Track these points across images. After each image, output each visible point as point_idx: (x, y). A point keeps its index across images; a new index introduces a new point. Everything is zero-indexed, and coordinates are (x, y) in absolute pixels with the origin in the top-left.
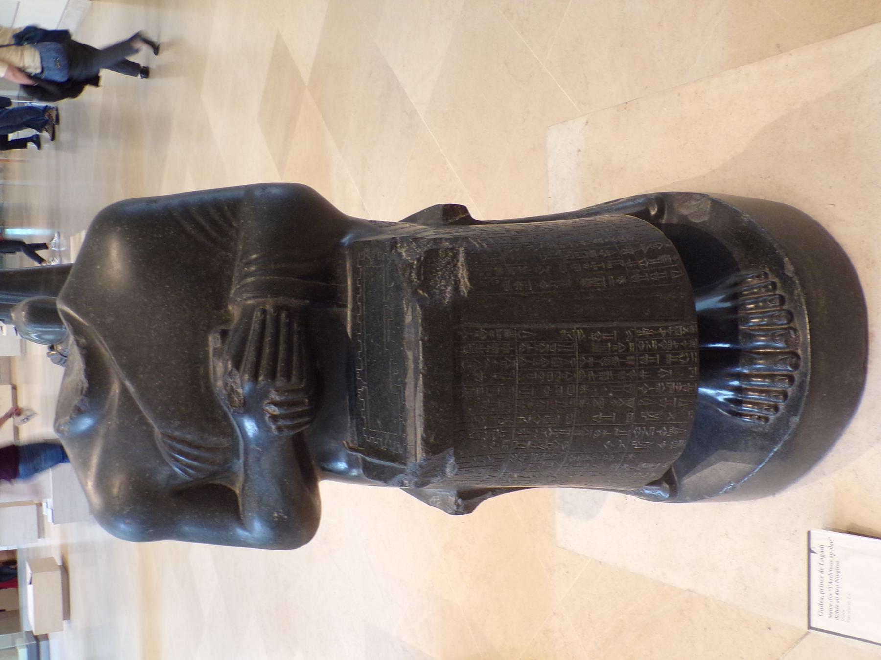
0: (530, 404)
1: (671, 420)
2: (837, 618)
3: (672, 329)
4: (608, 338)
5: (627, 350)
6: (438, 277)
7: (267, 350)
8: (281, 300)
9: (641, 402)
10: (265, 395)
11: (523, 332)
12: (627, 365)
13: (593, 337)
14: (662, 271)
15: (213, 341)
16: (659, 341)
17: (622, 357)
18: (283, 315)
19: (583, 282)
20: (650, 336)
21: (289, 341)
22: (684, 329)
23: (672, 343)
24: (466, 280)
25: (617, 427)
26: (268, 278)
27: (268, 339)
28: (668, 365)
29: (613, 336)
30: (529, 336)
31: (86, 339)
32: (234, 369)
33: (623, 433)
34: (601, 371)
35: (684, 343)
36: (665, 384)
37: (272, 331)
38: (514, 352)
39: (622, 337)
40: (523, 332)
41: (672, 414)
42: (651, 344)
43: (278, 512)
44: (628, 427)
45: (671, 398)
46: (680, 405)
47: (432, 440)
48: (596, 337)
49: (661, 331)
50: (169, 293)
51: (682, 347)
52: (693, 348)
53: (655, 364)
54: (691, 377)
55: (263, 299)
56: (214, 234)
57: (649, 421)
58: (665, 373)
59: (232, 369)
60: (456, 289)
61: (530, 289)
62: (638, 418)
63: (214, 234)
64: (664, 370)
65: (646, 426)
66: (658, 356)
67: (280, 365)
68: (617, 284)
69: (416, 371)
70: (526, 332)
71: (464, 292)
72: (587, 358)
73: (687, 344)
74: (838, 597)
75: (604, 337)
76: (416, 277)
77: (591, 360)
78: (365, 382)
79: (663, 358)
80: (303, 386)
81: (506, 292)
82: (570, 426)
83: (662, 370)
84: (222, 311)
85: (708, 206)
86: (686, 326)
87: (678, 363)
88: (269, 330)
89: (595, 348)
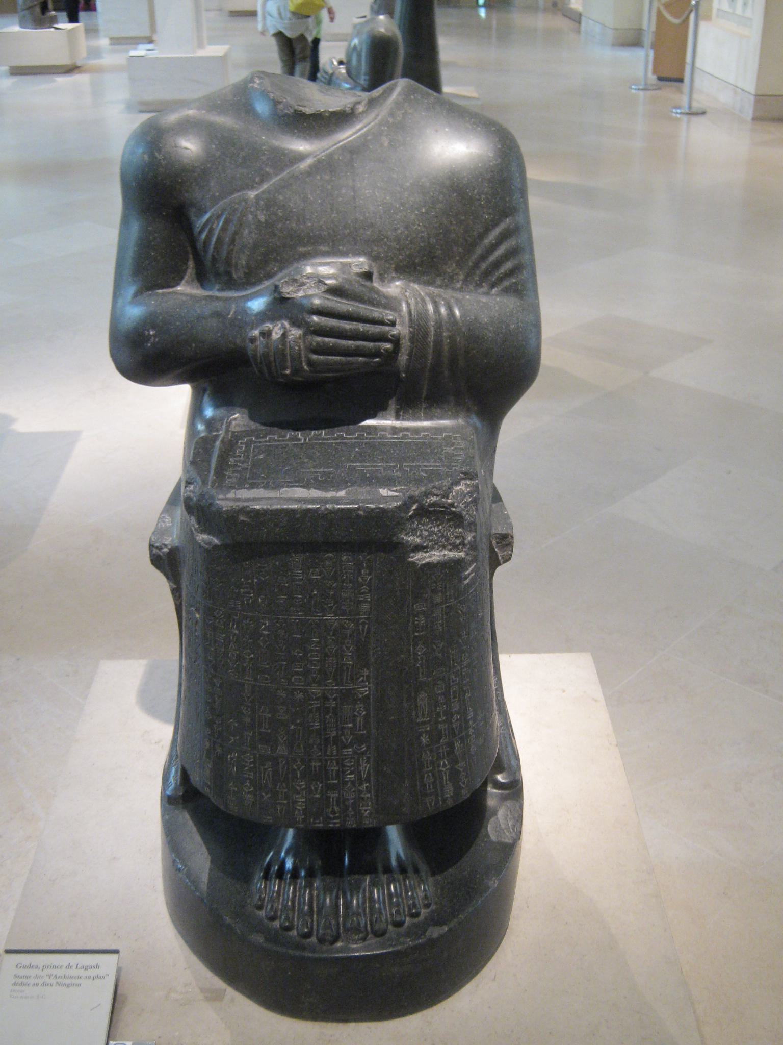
1: (262, 797)
3: (368, 797)
7: (347, 325)
8: (405, 344)
10: (295, 323)
11: (366, 626)
13: (360, 706)
16: (353, 782)
17: (336, 740)
19: (423, 695)
21: (357, 352)
22: (368, 812)
24: (428, 560)
25: (254, 733)
27: (361, 327)
34: (320, 715)
39: (360, 740)
40: (366, 626)
42: (351, 773)
43: (155, 336)
45: (286, 798)
47: (242, 518)
56: (484, 266)
58: (316, 789)
59: (326, 284)
60: (418, 548)
61: (416, 634)
63: (484, 266)
66: (336, 782)
69: (326, 501)
72: (335, 699)
75: (359, 719)
81: (413, 605)
82: (256, 679)
85: (507, 839)
87: (328, 807)
89: (347, 708)
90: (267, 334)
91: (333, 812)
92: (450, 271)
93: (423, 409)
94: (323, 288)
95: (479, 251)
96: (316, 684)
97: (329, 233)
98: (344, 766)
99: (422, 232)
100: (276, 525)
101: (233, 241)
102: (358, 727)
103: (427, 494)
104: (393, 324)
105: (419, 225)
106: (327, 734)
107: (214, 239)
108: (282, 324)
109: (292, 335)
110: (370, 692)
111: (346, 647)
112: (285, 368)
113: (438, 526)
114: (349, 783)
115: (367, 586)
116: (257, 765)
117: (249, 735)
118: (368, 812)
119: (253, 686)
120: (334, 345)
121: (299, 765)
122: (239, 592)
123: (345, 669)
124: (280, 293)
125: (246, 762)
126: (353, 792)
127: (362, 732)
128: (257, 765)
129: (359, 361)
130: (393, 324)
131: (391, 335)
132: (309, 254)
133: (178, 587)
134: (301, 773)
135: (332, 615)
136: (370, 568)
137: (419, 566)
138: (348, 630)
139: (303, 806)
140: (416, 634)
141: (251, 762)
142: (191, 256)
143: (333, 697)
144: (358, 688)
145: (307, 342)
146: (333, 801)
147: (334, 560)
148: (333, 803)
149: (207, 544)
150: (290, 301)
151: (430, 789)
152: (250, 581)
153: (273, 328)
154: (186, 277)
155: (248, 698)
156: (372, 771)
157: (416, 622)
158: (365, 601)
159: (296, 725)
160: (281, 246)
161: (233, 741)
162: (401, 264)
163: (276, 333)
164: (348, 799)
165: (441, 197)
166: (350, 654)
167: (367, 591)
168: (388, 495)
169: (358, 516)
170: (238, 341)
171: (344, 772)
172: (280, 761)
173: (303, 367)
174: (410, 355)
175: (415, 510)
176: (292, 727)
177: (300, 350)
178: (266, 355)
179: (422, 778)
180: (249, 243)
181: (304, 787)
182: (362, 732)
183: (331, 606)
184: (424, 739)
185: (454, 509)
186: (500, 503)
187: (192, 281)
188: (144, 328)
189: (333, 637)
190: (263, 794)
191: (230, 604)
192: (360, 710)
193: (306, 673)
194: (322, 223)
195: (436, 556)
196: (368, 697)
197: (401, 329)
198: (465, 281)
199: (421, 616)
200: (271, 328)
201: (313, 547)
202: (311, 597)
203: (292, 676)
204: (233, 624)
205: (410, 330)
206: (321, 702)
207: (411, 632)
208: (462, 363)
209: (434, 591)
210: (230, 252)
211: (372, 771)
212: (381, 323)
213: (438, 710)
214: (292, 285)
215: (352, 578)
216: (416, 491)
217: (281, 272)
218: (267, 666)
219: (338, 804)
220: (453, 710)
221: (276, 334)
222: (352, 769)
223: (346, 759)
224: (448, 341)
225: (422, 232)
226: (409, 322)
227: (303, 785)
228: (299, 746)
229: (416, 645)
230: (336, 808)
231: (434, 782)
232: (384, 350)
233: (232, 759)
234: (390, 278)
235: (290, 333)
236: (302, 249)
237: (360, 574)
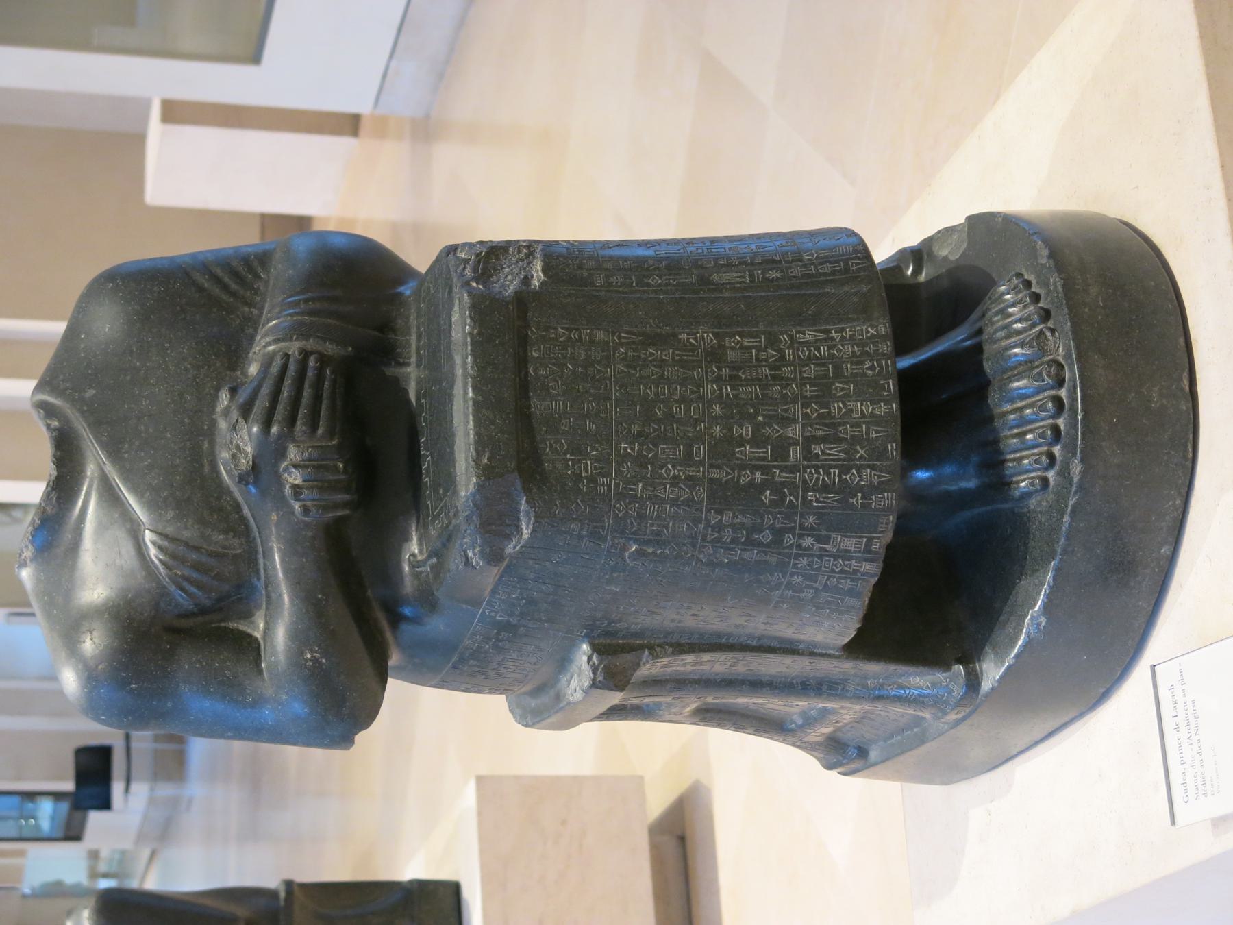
0: (636, 428)
1: (861, 457)
3: (850, 331)
4: (751, 344)
5: (782, 357)
8: (311, 344)
9: (808, 431)
10: (281, 453)
11: (623, 335)
12: (782, 379)
14: (837, 262)
15: (224, 398)
16: (830, 348)
18: (312, 362)
20: (816, 341)
22: (870, 329)
24: (540, 273)
25: (774, 467)
26: (295, 318)
27: (285, 393)
28: (847, 377)
29: (829, 413)
31: (59, 421)
32: (240, 420)
33: (787, 477)
34: (741, 385)
36: (844, 404)
37: (293, 374)
38: (608, 358)
39: (773, 341)
40: (623, 335)
41: (862, 449)
42: (819, 351)
43: (312, 652)
44: (794, 469)
45: (859, 425)
46: (873, 435)
47: (485, 461)
49: (834, 334)
50: (169, 352)
51: (864, 353)
52: (883, 354)
53: (826, 376)
54: (885, 393)
55: (287, 344)
56: (234, 286)
57: (826, 460)
58: (842, 389)
61: (634, 284)
63: (234, 286)
64: (841, 385)
65: (823, 467)
66: (830, 366)
67: (303, 412)
69: (465, 376)
70: (626, 336)
72: (719, 369)
73: (875, 349)
75: (746, 344)
77: (726, 372)
79: (838, 369)
80: (333, 443)
81: (597, 287)
82: (702, 463)
83: (837, 385)
84: (239, 373)
87: (864, 375)
89: (733, 356)
90: (296, 489)
91: (872, 368)
92: (239, 320)
93: (397, 338)
94: (242, 423)
95: (216, 291)
96: (699, 389)
97: (188, 440)
98: (809, 358)
99: (191, 343)
100: (493, 423)
101: (197, 549)
102: (757, 344)
104: (287, 356)
105: (183, 348)
107: (195, 575)
109: (295, 457)
110: (710, 332)
111: (649, 357)
112: (336, 467)
113: (503, 268)
115: (571, 332)
116: (819, 463)
118: (870, 329)
119: (711, 466)
121: (811, 410)
123: (678, 358)
124: (248, 473)
125: (818, 479)
126: (842, 347)
127: (763, 340)
130: (287, 356)
131: (299, 356)
132: (211, 461)
133: (648, 648)
134: (822, 408)
136: (548, 328)
138: (629, 354)
140: (634, 284)
141: (815, 473)
142: (223, 624)
143: (716, 370)
144: (704, 344)
145: (302, 439)
146: (856, 369)
147: (538, 365)
148: (859, 369)
149: (530, 519)
150: (256, 461)
154: (249, 631)
155: (727, 474)
156: (814, 328)
158: (591, 334)
159: (757, 414)
160: (201, 491)
161: (791, 498)
162: (227, 365)
163: (295, 479)
164: (852, 352)
165: (155, 330)
166: (659, 352)
167: (577, 333)
170: (310, 534)
171: (817, 358)
172: (809, 434)
174: (324, 340)
175: (478, 284)
176: (760, 418)
177: (313, 447)
179: (825, 274)
180: (199, 529)
181: (841, 405)
182: (763, 340)
183: (719, 520)
185: (483, 253)
187: (253, 623)
188: (303, 666)
189: (638, 369)
190: (858, 456)
192: (734, 342)
194: (176, 448)
196: (716, 335)
198: (251, 305)
199: (611, 280)
200: (290, 485)
201: (523, 388)
203: (691, 417)
204: (631, 490)
205: (295, 340)
206: (724, 385)
207: (633, 289)
210: (212, 554)
211: (814, 328)
214: (239, 460)
215: (560, 348)
217: (232, 493)
218: (682, 447)
219: (862, 363)
222: (812, 349)
223: (799, 356)
224: (310, 303)
225: (191, 343)
226: (287, 341)
227: (838, 406)
228: (786, 411)
229: (648, 285)
230: (868, 364)
232: (316, 363)
233: (817, 501)
235: (294, 460)
236: (206, 469)
237: (555, 339)
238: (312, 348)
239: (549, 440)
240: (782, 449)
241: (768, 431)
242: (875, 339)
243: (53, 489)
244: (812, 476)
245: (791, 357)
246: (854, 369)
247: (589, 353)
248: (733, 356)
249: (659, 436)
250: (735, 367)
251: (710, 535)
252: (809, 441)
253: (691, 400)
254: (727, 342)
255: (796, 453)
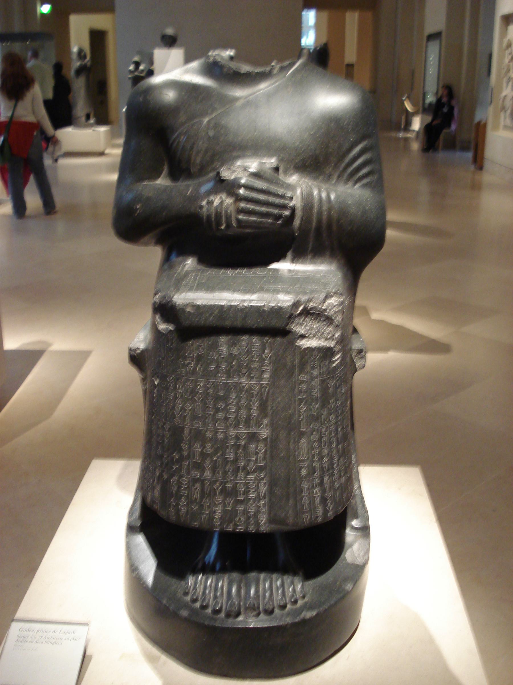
0: (211, 391)
2: (17, 641)
6: (311, 325)
7: (262, 197)
8: (299, 214)
13: (261, 445)
17: (244, 468)
19: (303, 441)
21: (267, 215)
23: (252, 510)
27: (271, 199)
30: (263, 393)
35: (251, 521)
39: (260, 469)
48: (260, 449)
51: (249, 518)
59: (249, 172)
60: (303, 337)
62: (195, 480)
65: (188, 487)
68: (301, 469)
71: (300, 343)
74: (34, 642)
76: (312, 306)
77: (242, 442)
78: (234, 275)
79: (242, 502)
85: (359, 561)
86: (265, 523)
88: (277, 201)
89: (252, 447)
98: (249, 488)
103: (310, 300)
106: (238, 464)
108: (221, 197)
114: (251, 501)
117: (185, 464)
120: (253, 209)
122: (184, 363)
128: (190, 486)
129: (268, 222)
130: (291, 198)
135: (244, 380)
137: (303, 349)
139: (219, 515)
151: (306, 509)
152: (192, 355)
153: (215, 200)
154: (162, 176)
157: (300, 389)
161: (174, 469)
168: (284, 299)
169: (263, 310)
173: (232, 224)
178: (209, 217)
181: (220, 501)
182: (261, 464)
184: (304, 472)
186: (359, 335)
191: (178, 372)
193: (226, 419)
195: (313, 343)
196: (266, 439)
197: (297, 202)
202: (232, 367)
208: (335, 228)
209: (313, 368)
212: (283, 197)
213: (313, 453)
216: (303, 298)
220: (323, 455)
221: (217, 202)
223: (249, 483)
227: (220, 500)
231: (310, 503)
234: (289, 174)
238: (296, 213)
239: (204, 344)
240: (199, 467)
241: (208, 461)
242: (257, 523)
243: (234, 71)
244: (185, 480)
245: (249, 479)
246: (240, 511)
247: (255, 370)
248: (252, 447)
249: (207, 404)
250: (245, 447)
251: (160, 424)
252: (202, 482)
253: (226, 423)
254: (261, 445)
255: (195, 474)
